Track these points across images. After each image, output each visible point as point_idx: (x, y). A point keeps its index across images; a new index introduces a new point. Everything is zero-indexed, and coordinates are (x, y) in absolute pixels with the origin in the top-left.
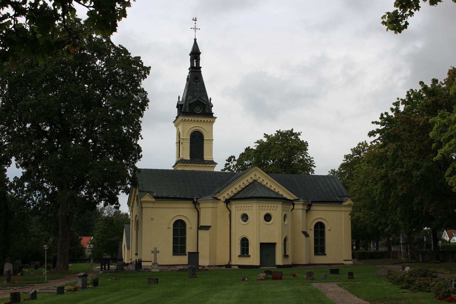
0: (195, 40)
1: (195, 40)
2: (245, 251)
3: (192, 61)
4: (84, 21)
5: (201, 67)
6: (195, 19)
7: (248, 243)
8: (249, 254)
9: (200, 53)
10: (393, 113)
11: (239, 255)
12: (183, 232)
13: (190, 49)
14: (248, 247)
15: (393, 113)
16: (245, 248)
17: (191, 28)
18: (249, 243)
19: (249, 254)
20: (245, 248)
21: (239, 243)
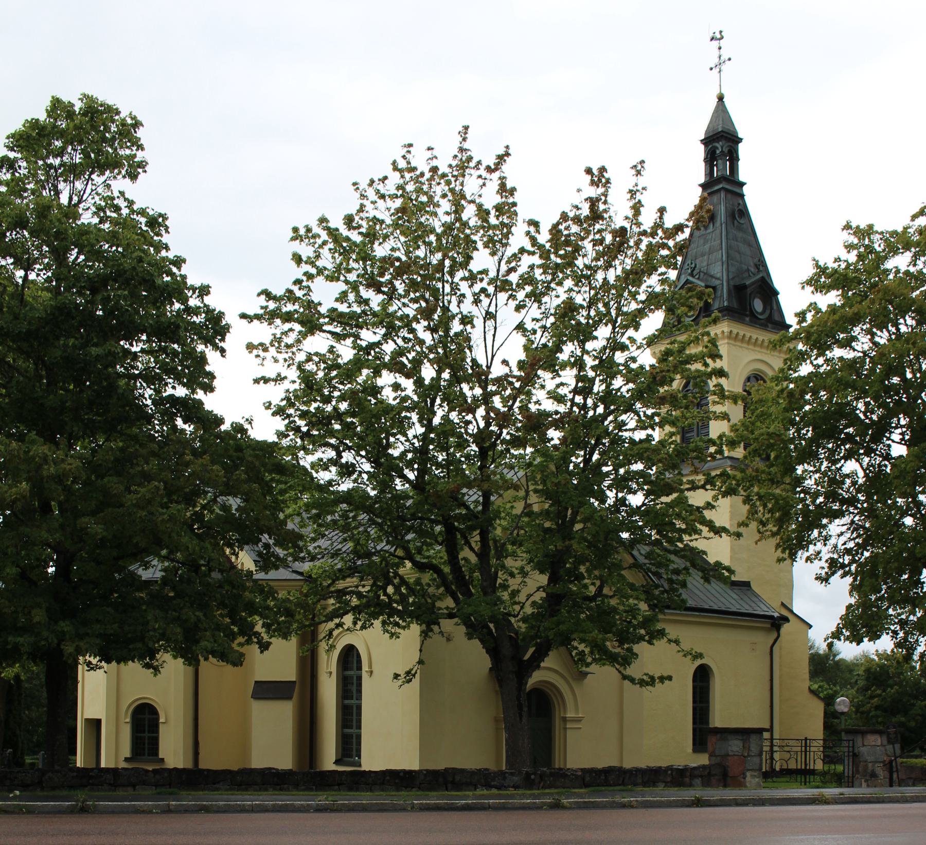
0: (721, 98)
1: (721, 98)
2: (146, 746)
3: (711, 159)
4: (139, 173)
5: (700, 185)
6: (719, 36)
7: (158, 719)
8: (161, 756)
9: (740, 140)
10: (807, 297)
11: (128, 755)
12: (154, 726)
13: (700, 128)
14: (157, 731)
15: (807, 297)
16: (146, 735)
17: (730, 59)
18: (162, 720)
19: (161, 756)
20: (146, 735)
21: (128, 720)
